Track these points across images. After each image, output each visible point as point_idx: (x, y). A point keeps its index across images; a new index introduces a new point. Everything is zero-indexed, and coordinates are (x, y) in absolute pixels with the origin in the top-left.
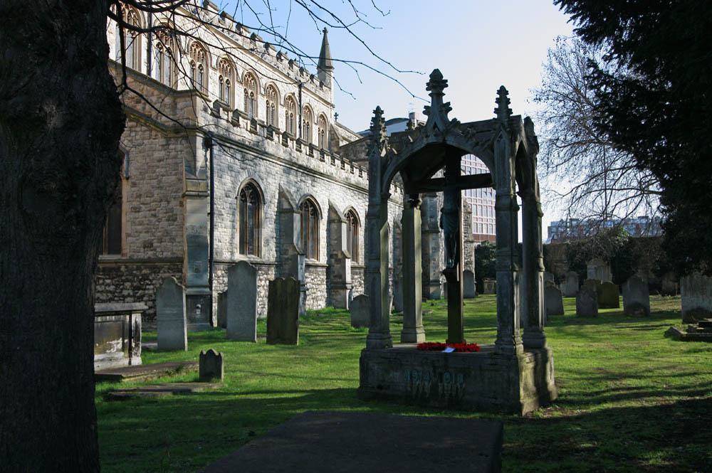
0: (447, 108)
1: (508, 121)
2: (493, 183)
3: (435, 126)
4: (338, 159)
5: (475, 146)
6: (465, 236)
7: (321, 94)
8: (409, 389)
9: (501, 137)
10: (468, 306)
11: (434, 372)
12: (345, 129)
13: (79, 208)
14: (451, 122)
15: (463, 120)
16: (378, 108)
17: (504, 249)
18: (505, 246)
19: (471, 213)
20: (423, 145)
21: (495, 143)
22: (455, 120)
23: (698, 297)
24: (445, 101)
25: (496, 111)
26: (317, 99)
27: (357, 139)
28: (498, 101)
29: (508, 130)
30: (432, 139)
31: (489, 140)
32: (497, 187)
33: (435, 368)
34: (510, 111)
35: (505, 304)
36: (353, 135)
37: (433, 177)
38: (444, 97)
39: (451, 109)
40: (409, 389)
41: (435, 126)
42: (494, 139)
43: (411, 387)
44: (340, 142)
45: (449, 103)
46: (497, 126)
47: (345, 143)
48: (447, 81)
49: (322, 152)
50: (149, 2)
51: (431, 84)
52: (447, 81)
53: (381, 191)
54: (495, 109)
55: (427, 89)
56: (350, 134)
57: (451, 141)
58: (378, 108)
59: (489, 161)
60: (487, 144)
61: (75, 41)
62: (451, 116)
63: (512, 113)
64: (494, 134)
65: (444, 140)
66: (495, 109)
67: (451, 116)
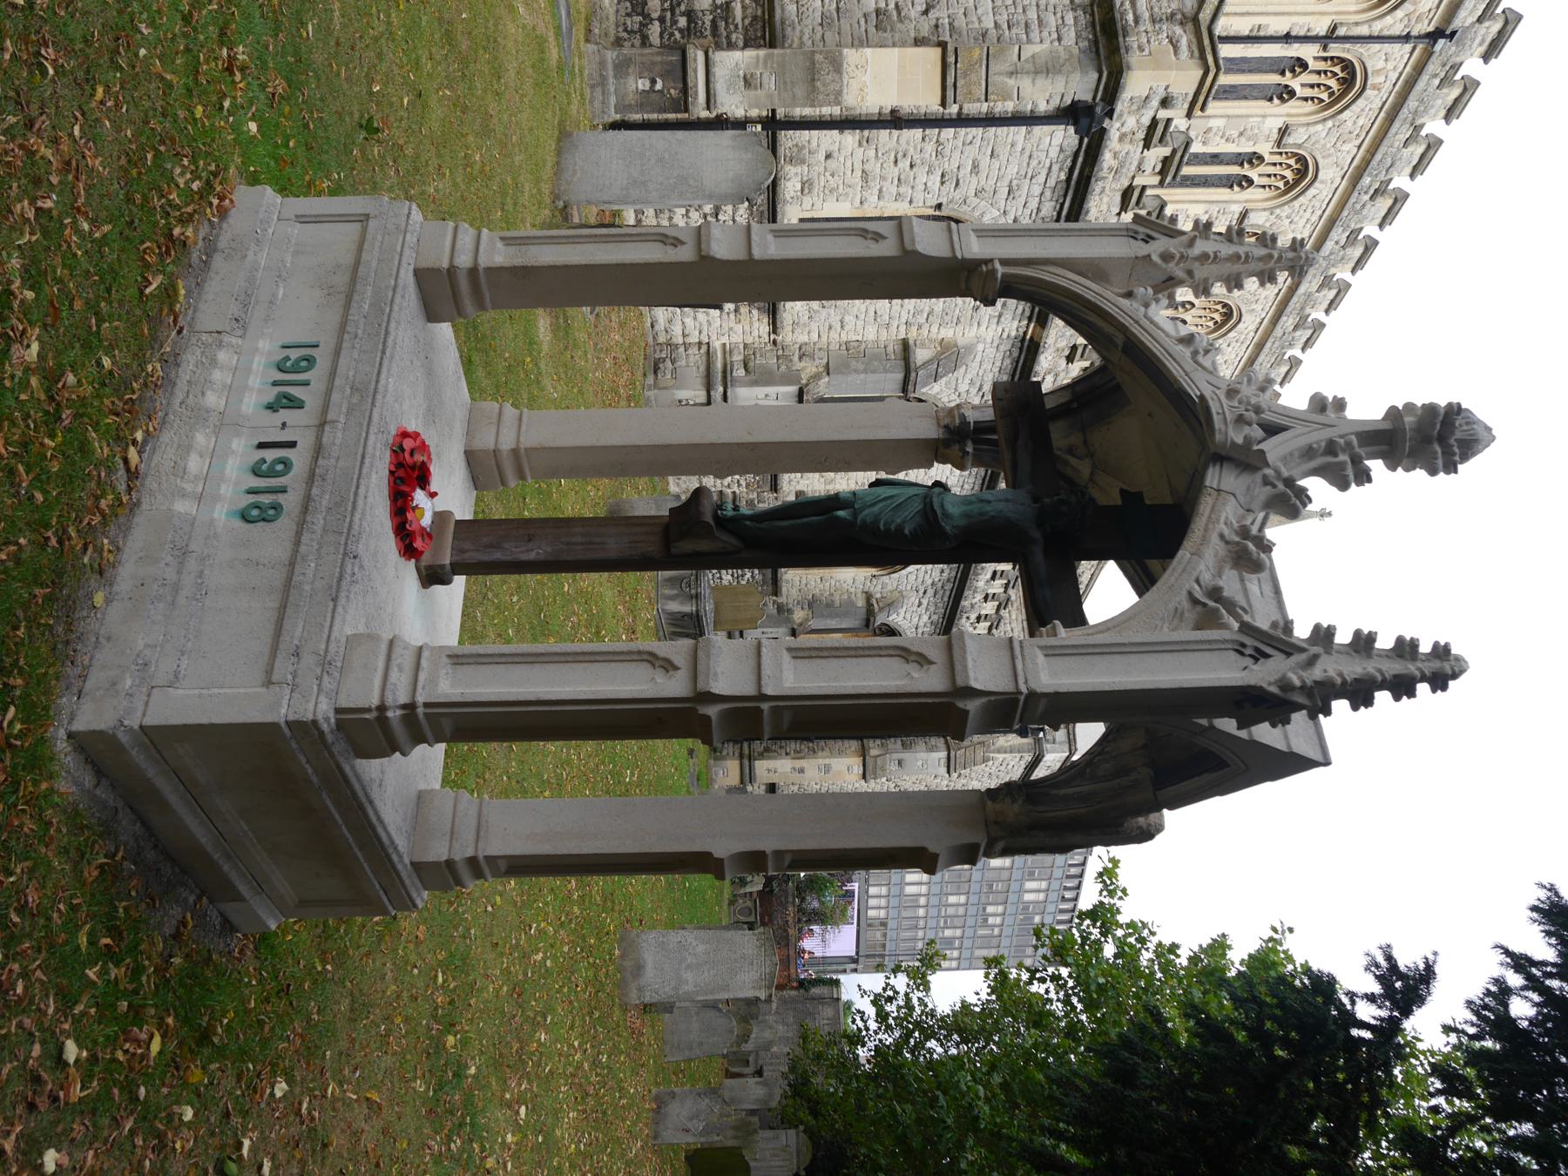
28: (1406, 648)
48: (1456, 472)
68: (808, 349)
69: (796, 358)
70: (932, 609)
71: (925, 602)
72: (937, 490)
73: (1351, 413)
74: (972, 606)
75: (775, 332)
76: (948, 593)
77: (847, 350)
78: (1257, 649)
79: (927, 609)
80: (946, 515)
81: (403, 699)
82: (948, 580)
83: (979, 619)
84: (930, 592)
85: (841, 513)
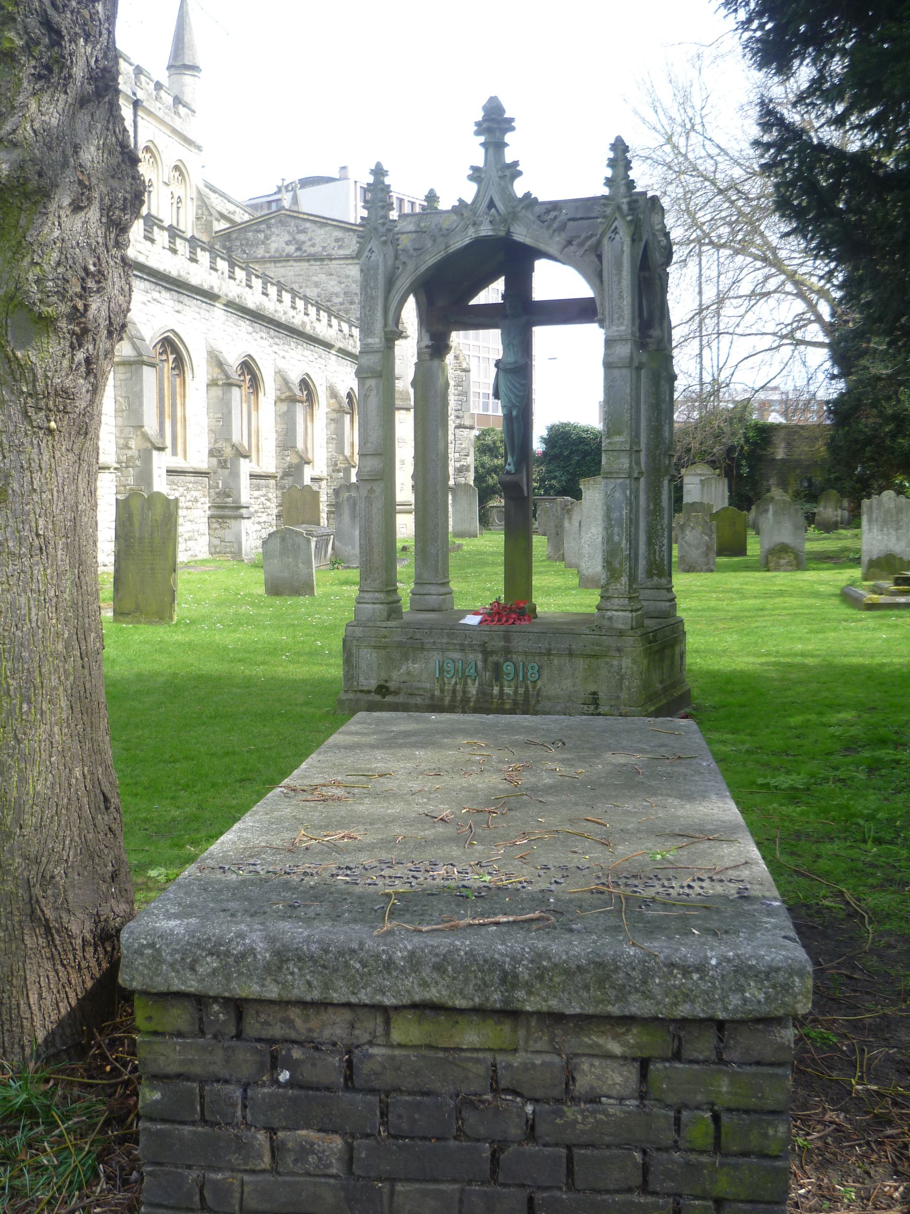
0: (512, 171)
1: (629, 203)
2: (600, 317)
3: (491, 204)
4: (222, 258)
5: (565, 247)
6: (458, 417)
7: (177, 124)
8: (437, 693)
9: (615, 231)
10: (186, 576)
11: (485, 661)
12: (223, 195)
13: (91, 347)
14: (521, 200)
15: (543, 196)
16: (379, 165)
17: (617, 439)
18: (620, 433)
19: (469, 371)
20: (467, 241)
21: (605, 241)
22: (528, 195)
23: (889, 534)
24: (509, 160)
25: (609, 182)
26: (169, 133)
27: (247, 217)
28: (612, 163)
29: (629, 218)
30: (486, 230)
31: (592, 236)
32: (607, 323)
33: (486, 653)
34: (631, 184)
35: (616, 538)
36: (238, 210)
37: (473, 302)
38: (507, 150)
39: (520, 173)
40: (437, 693)
41: (491, 204)
42: (603, 235)
43: (442, 691)
44: (215, 223)
45: (516, 164)
46: (609, 210)
47: (222, 225)
48: (512, 120)
49: (193, 242)
50: (901, 120)
51: (484, 125)
52: (512, 120)
53: (386, 325)
54: (607, 178)
55: (477, 133)
56: (232, 208)
57: (521, 234)
58: (379, 165)
59: (596, 277)
60: (589, 243)
61: (83, 50)
62: (520, 188)
63: (635, 187)
64: (604, 227)
65: (508, 232)
66: (607, 178)
67: (520, 188)
68: (121, 441)
69: (130, 453)
70: (286, 347)
71: (282, 353)
72: (501, 365)
73: (480, 163)
74: (285, 313)
75: (108, 468)
76: (276, 333)
77: (123, 411)
78: (613, 232)
79: (287, 352)
80: (515, 362)
81: (626, 601)
82: (268, 333)
83: (294, 308)
84: (275, 348)
85: (514, 413)
